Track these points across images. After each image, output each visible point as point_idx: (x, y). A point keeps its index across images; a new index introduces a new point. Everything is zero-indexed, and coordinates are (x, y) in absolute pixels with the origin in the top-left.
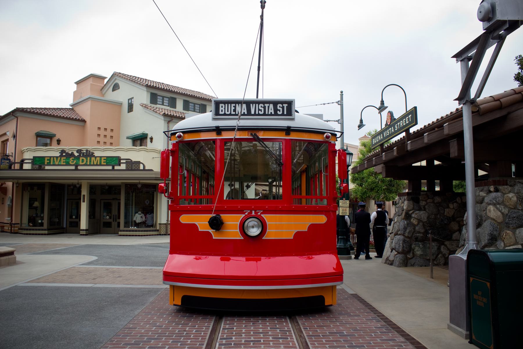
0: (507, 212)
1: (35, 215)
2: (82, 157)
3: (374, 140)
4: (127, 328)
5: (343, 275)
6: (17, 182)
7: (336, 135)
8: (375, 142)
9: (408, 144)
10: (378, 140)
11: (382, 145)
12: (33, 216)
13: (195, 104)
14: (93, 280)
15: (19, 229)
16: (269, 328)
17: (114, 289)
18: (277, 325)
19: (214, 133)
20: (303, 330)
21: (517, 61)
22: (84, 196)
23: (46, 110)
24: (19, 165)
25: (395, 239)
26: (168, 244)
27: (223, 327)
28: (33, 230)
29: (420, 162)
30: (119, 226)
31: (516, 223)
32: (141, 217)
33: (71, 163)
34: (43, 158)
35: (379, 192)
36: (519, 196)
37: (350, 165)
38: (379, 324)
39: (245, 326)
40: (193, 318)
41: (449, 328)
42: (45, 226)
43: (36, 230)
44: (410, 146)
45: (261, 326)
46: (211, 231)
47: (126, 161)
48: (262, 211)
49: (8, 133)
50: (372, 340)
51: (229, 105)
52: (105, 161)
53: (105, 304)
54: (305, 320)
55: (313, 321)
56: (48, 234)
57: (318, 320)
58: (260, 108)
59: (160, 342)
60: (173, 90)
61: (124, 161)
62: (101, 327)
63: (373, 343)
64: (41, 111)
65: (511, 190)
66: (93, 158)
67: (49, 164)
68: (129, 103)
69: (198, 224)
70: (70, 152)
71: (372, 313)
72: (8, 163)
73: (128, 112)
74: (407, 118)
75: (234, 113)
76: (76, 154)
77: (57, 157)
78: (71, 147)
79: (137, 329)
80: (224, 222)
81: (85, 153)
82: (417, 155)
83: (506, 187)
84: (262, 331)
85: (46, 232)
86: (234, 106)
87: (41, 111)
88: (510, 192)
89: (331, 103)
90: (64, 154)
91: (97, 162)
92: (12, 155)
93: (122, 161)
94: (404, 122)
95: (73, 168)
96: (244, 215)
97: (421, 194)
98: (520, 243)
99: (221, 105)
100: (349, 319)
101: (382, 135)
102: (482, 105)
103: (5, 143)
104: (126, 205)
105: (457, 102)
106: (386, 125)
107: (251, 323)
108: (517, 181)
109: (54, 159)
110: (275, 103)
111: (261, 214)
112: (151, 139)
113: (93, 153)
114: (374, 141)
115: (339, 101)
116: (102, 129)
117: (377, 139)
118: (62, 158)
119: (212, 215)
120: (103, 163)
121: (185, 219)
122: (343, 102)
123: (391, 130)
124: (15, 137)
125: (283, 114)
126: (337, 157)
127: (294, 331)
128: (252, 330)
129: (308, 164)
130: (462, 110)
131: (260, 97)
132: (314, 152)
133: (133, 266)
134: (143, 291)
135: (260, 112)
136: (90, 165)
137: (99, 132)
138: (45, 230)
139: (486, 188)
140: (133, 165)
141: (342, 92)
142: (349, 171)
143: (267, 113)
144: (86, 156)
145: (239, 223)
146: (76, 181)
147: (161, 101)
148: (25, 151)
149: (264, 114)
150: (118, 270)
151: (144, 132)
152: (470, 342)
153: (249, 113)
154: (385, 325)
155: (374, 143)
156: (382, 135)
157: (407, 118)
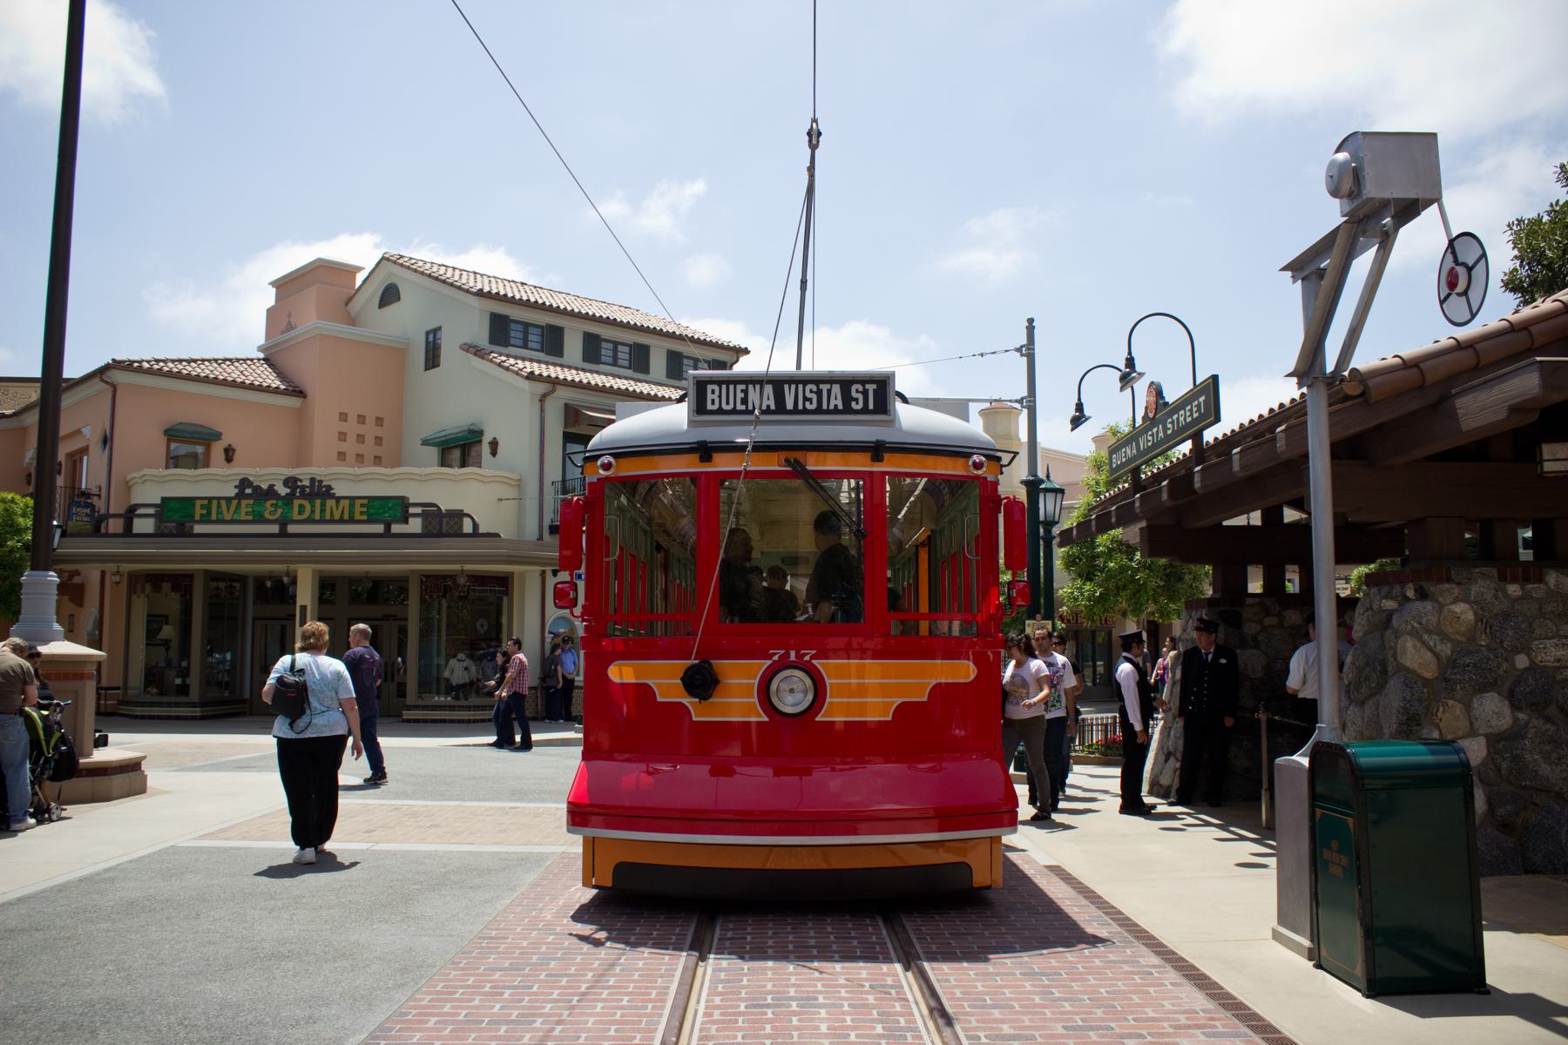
0: (1449, 652)
1: (164, 664)
2: (298, 498)
3: (1114, 456)
4: (484, 938)
5: (1017, 813)
6: (116, 570)
7: (999, 459)
8: (1119, 463)
9: (1196, 475)
10: (1125, 456)
11: (1136, 471)
12: (160, 665)
13: (616, 344)
14: (368, 834)
15: (121, 703)
16: (832, 937)
17: (429, 855)
18: (852, 932)
19: (695, 457)
20: (915, 941)
21: (1512, 234)
22: (304, 608)
23: (193, 364)
24: (120, 522)
25: (1175, 725)
26: (750, 695)
27: (720, 934)
28: (160, 704)
29: (1246, 516)
30: (401, 691)
31: (1470, 679)
32: (466, 669)
33: (267, 516)
34: (190, 501)
35: (1138, 595)
36: (1481, 608)
37: (1057, 523)
38: (1104, 931)
39: (773, 933)
40: (639, 926)
41: (1276, 936)
42: (194, 694)
43: (169, 705)
44: (1199, 479)
45: (812, 934)
46: (690, 702)
47: (423, 511)
48: (814, 652)
49: (86, 431)
50: (1082, 962)
51: (732, 387)
52: (365, 509)
53: (415, 887)
54: (921, 921)
55: (940, 924)
56: (202, 718)
57: (955, 921)
58: (808, 395)
59: (572, 965)
60: (555, 305)
61: (418, 510)
62: (420, 936)
63: (1143, 1035)
64: (180, 367)
65: (1459, 594)
66: (330, 503)
67: (205, 520)
68: (427, 342)
69: (658, 685)
70: (265, 486)
71: (1092, 906)
72: (87, 515)
73: (427, 369)
74: (1196, 403)
75: (743, 407)
76: (283, 491)
77: (228, 500)
78: (271, 475)
79: (509, 940)
80: (720, 679)
81: (307, 487)
82: (1236, 495)
83: (1447, 586)
84: (816, 942)
85: (197, 711)
86: (742, 391)
87: (180, 367)
88: (1456, 601)
89: (1000, 352)
90: (248, 491)
91: (343, 512)
92: (98, 493)
93: (412, 510)
94: (1188, 414)
95: (275, 529)
96: (769, 662)
97: (1247, 603)
98: (1481, 732)
99: (710, 388)
100: (1033, 920)
101: (1134, 444)
102: (1373, 380)
103: (77, 457)
104: (425, 634)
105: (1295, 380)
106: (1145, 418)
107: (789, 928)
108: (1477, 570)
109: (219, 506)
110: (846, 382)
111: (811, 658)
112: (494, 445)
113: (329, 488)
114: (1114, 460)
115: (1022, 347)
116: (352, 418)
117: (1123, 455)
118: (244, 502)
119: (689, 662)
120: (357, 517)
121: (621, 673)
122: (1033, 349)
123: (1157, 432)
124: (107, 441)
125: (865, 410)
126: (1002, 514)
127: (892, 943)
128: (791, 942)
129: (933, 528)
130: (1305, 401)
131: (806, 367)
132: (948, 495)
133: (463, 800)
134: (506, 859)
135: (807, 404)
136: (322, 521)
137: (343, 427)
138: (193, 705)
139: (1397, 589)
140: (443, 523)
141: (1031, 321)
142: (1055, 537)
143: (825, 407)
144: (309, 495)
145: (756, 681)
146: (281, 567)
147: (520, 335)
148: (136, 483)
149: (819, 410)
150: (425, 809)
151: (472, 427)
152: (1319, 966)
153: (781, 408)
154: (1119, 933)
155: (1114, 466)
156: (1134, 444)
157: (1196, 403)
